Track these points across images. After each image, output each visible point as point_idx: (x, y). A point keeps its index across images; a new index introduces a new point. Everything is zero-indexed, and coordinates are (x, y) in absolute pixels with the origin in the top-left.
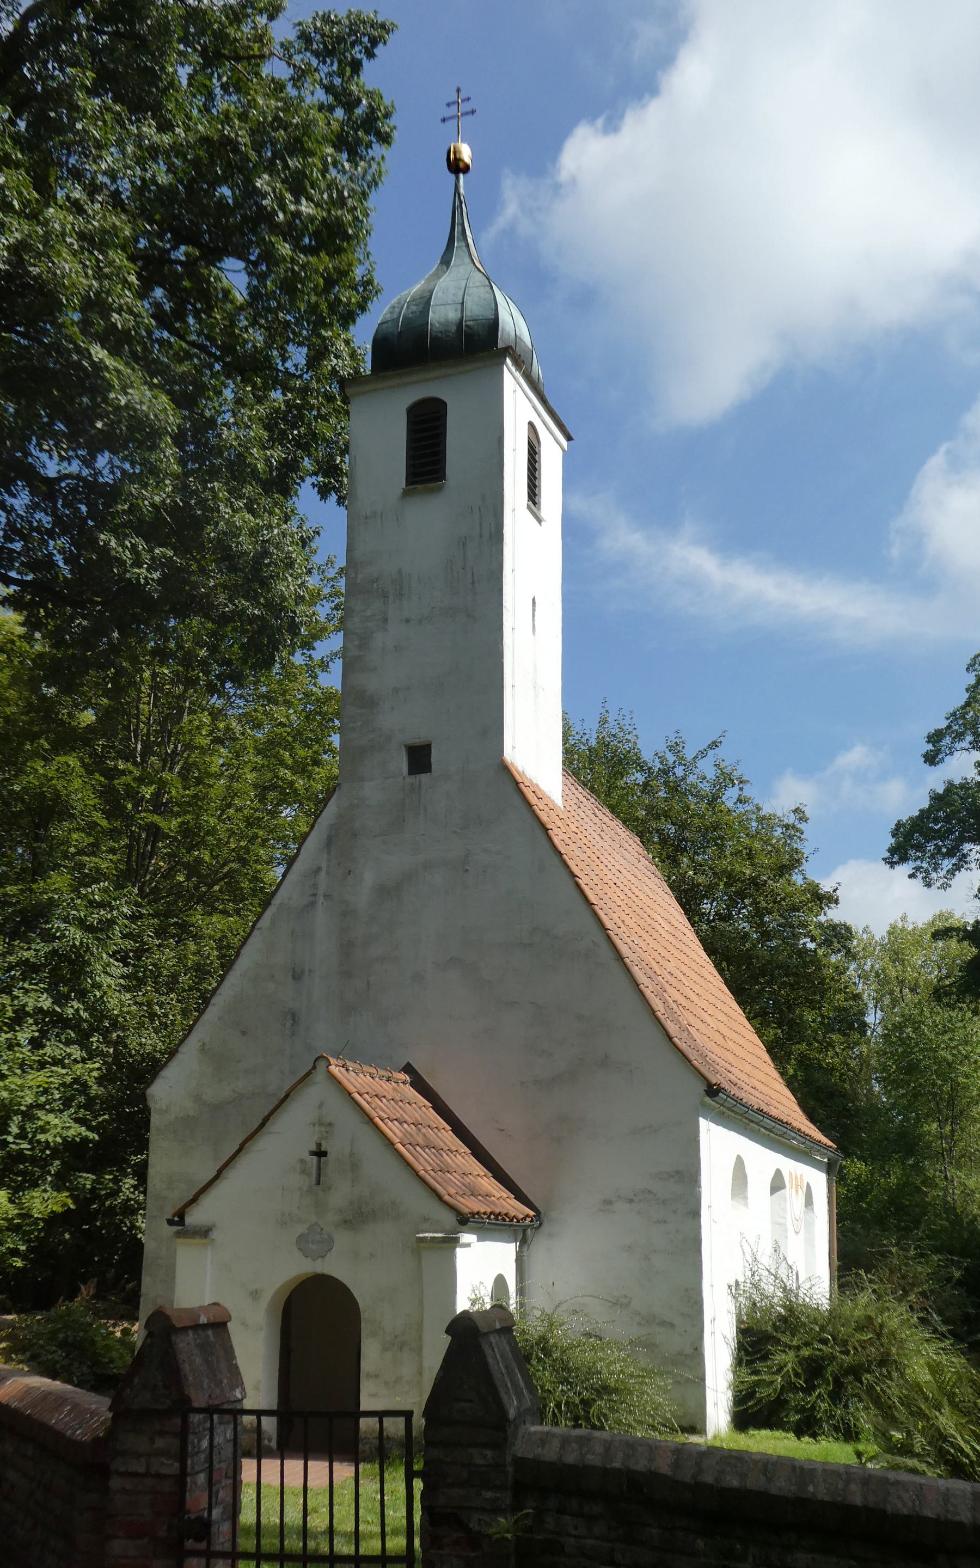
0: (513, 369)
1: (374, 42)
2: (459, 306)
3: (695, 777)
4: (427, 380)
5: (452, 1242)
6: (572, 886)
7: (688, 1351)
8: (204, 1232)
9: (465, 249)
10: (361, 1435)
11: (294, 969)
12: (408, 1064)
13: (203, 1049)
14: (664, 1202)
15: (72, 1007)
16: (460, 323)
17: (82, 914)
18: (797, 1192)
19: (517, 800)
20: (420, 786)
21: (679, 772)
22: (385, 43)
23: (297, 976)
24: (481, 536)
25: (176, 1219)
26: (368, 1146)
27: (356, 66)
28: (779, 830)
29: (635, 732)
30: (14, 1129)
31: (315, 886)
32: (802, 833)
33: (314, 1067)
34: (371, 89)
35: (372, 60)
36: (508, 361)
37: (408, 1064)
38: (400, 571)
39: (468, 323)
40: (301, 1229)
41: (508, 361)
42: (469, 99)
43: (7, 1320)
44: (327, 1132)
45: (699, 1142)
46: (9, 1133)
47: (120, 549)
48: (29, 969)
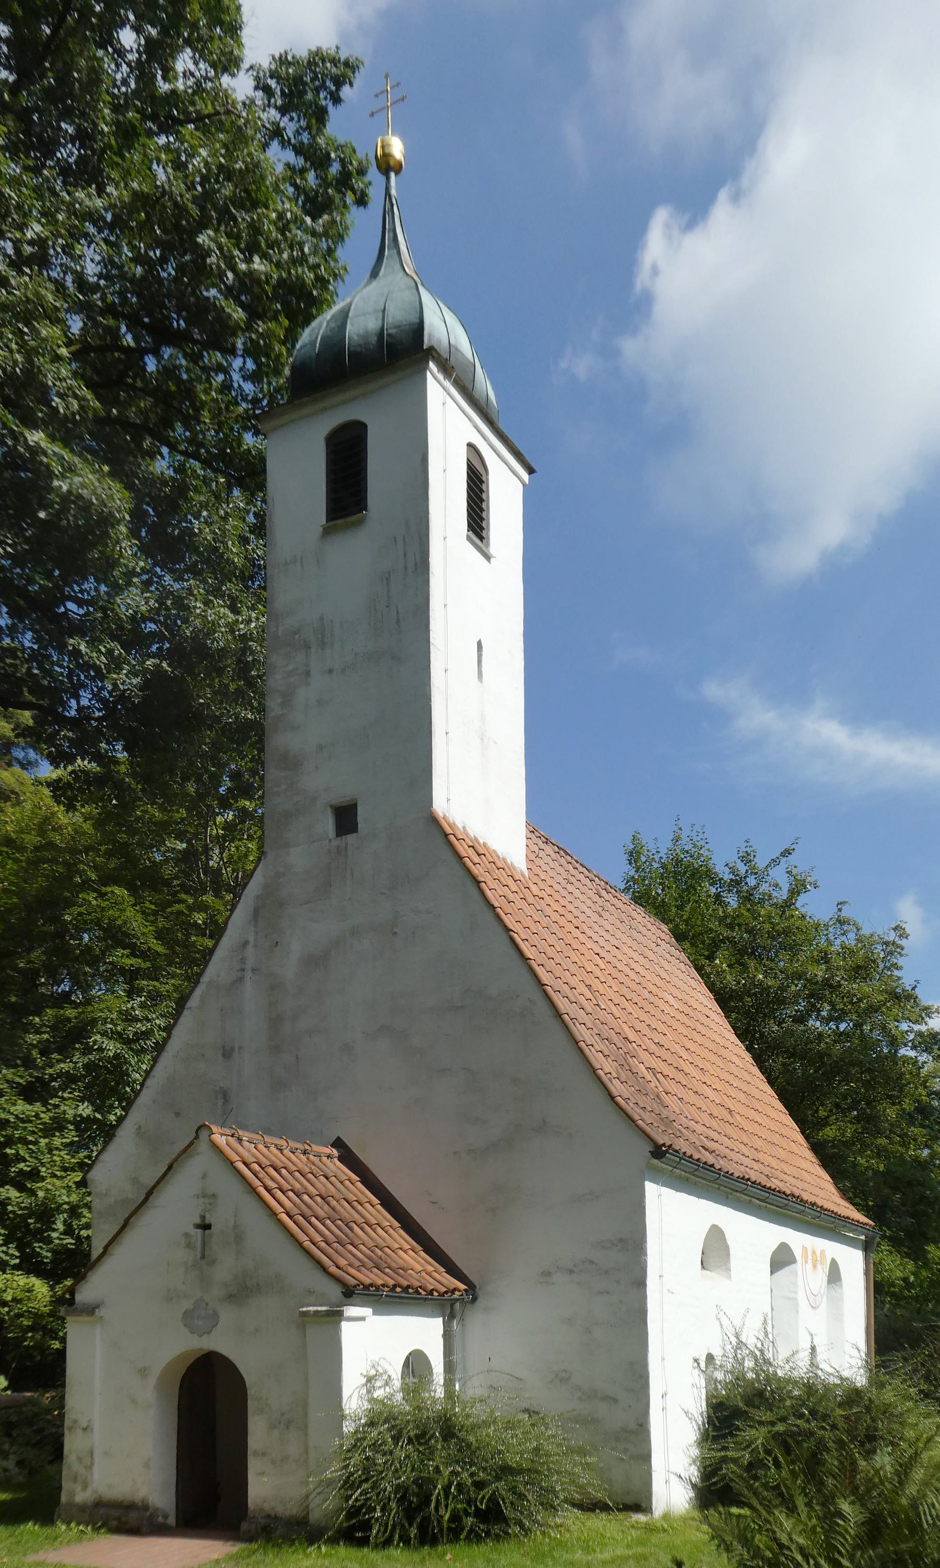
0: (440, 376)
1: (339, 82)
2: (380, 314)
3: (767, 884)
4: (343, 403)
5: (335, 1316)
6: (507, 940)
7: (633, 1426)
8: (91, 1310)
9: (396, 256)
10: (250, 1514)
11: (224, 1047)
12: (339, 1138)
13: (139, 1132)
14: (606, 1272)
15: (116, 1114)
16: (381, 334)
17: (119, 1028)
18: (815, 1267)
19: (447, 854)
20: (346, 847)
21: (752, 881)
22: (351, 85)
23: (227, 1053)
24: (406, 568)
25: (68, 1296)
26: (252, 1216)
27: (320, 116)
28: (880, 947)
29: (707, 846)
30: (60, 1226)
31: (243, 960)
32: (902, 949)
33: (197, 1137)
34: (342, 143)
35: (338, 106)
36: (432, 365)
37: (339, 1138)
38: (322, 619)
39: (390, 331)
40: (187, 1304)
41: (432, 365)
42: (398, 84)
43: (24, 1397)
44: (210, 1204)
45: (644, 1208)
46: (54, 1230)
47: (94, 654)
48: (69, 1079)
